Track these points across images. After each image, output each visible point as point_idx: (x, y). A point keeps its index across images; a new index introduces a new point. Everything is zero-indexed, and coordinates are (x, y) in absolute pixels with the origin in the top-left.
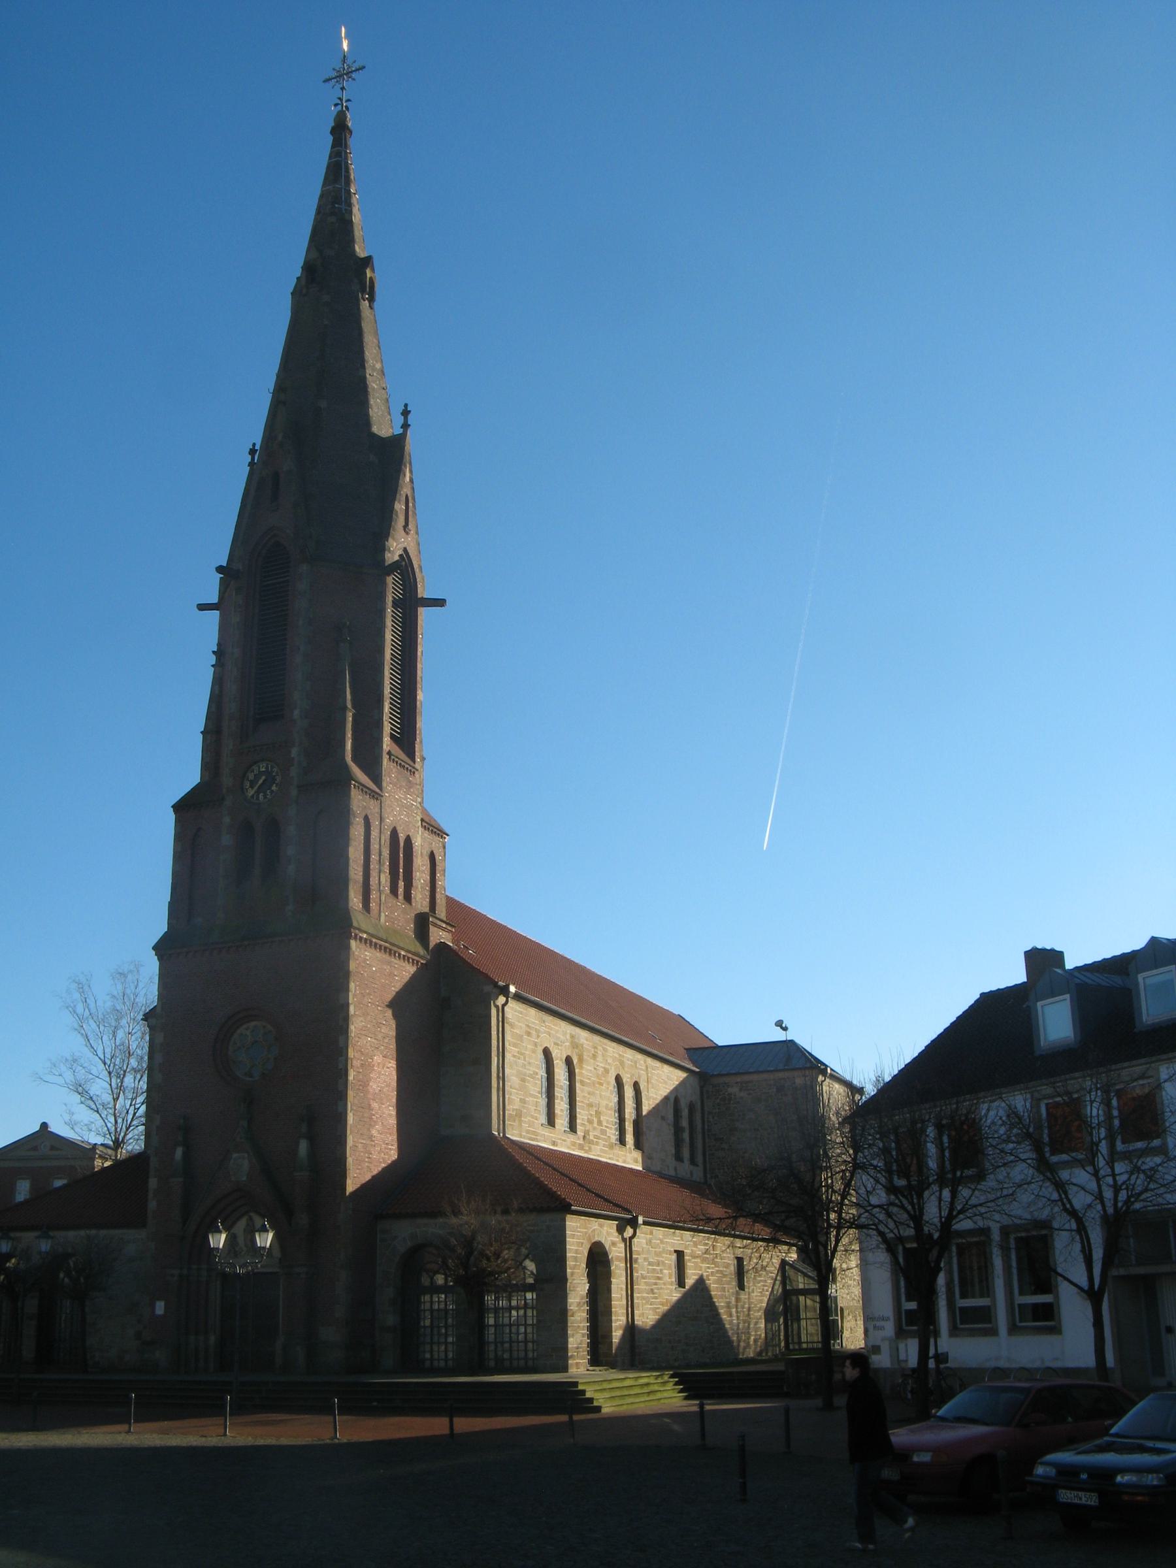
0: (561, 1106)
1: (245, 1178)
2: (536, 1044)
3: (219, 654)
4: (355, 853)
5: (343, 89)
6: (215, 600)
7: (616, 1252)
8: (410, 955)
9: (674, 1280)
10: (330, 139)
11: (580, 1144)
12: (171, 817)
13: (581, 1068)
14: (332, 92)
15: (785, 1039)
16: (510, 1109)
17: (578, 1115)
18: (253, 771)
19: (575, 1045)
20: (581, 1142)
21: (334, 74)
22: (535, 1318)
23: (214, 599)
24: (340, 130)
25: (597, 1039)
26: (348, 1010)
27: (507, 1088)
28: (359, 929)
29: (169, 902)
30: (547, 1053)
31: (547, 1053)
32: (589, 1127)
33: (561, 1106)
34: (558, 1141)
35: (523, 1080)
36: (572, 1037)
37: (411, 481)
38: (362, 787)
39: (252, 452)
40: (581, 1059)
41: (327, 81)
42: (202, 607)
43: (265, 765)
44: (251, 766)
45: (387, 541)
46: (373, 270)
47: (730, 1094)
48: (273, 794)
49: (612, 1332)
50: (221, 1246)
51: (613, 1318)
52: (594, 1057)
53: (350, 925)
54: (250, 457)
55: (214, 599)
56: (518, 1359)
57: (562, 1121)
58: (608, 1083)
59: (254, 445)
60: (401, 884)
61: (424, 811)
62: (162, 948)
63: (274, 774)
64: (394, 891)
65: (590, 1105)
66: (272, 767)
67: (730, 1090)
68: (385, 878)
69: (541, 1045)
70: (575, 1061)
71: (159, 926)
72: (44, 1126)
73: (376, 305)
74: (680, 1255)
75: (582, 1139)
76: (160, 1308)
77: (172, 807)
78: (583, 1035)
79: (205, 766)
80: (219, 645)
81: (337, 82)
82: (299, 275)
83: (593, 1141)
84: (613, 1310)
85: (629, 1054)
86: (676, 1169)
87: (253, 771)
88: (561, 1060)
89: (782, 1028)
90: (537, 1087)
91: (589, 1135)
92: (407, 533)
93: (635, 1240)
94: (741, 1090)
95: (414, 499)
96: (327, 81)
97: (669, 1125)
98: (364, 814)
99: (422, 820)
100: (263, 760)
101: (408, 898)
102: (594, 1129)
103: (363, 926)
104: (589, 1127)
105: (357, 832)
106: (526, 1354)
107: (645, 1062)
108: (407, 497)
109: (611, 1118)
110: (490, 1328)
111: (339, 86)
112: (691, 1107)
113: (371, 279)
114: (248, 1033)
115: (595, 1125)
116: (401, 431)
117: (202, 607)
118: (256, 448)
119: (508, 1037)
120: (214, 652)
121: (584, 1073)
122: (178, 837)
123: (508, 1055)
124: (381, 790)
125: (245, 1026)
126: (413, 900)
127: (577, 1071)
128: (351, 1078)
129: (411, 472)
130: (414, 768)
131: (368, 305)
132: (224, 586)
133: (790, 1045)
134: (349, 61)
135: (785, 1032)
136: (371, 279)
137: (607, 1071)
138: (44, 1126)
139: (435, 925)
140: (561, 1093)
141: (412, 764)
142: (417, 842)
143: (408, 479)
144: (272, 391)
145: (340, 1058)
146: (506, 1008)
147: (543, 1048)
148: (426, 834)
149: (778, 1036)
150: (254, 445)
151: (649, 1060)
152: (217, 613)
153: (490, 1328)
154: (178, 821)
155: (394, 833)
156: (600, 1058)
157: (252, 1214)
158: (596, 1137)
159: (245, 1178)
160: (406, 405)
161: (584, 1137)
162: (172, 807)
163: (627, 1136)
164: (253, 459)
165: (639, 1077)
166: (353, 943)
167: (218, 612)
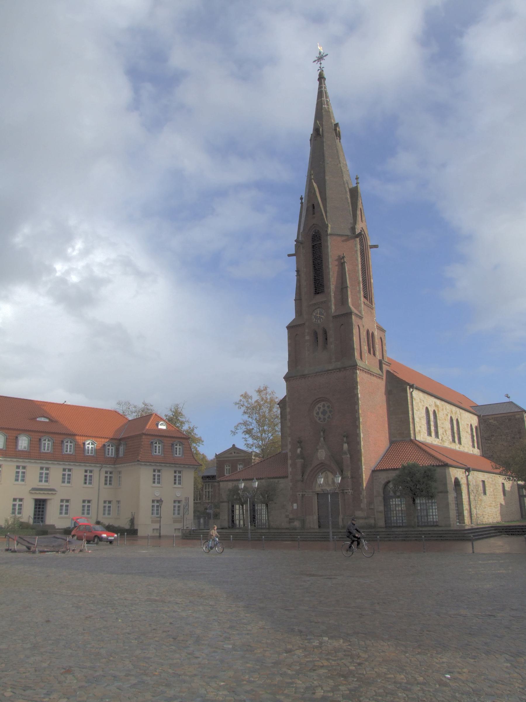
0: (433, 428)
1: (324, 459)
2: (423, 406)
3: (298, 271)
4: (356, 339)
5: (321, 64)
6: (294, 253)
7: (463, 482)
8: (377, 375)
9: (482, 491)
10: (318, 82)
11: (440, 442)
12: (286, 331)
13: (439, 414)
14: (317, 66)
15: (509, 401)
16: (417, 430)
17: (439, 432)
18: (315, 312)
19: (436, 406)
20: (441, 441)
21: (316, 59)
22: (266, 515)
23: (294, 252)
24: (321, 78)
25: (443, 403)
26: (358, 396)
27: (415, 422)
28: (360, 366)
29: (288, 361)
30: (427, 408)
31: (427, 408)
32: (443, 436)
33: (433, 428)
34: (432, 440)
35: (420, 419)
36: (435, 403)
37: (362, 203)
38: (356, 315)
39: (301, 199)
40: (438, 410)
41: (314, 61)
42: (289, 255)
43: (319, 310)
44: (314, 310)
45: (356, 225)
46: (339, 128)
47: (490, 423)
48: (323, 320)
49: (463, 511)
50: (339, 482)
51: (464, 506)
52: (443, 409)
53: (357, 365)
54: (301, 200)
55: (294, 252)
56: (394, 523)
57: (433, 434)
58: (448, 419)
59: (302, 196)
60: (372, 349)
61: (377, 323)
62: (287, 378)
63: (323, 313)
64: (369, 352)
65: (443, 428)
66: (322, 310)
67: (490, 421)
68: (365, 348)
69: (425, 406)
70: (437, 412)
71: (285, 370)
72: (234, 445)
73: (341, 140)
74: (483, 482)
75: (441, 440)
76: (295, 506)
77: (286, 327)
78: (438, 402)
79: (297, 312)
80: (297, 268)
81: (318, 61)
82: (312, 133)
83: (444, 441)
84: (463, 503)
85: (454, 409)
86: (473, 451)
87: (315, 312)
88: (432, 411)
89: (507, 397)
90: (424, 422)
91: (443, 439)
92: (362, 222)
93: (469, 477)
94: (494, 421)
95: (363, 210)
96: (314, 61)
97: (469, 434)
98: (357, 325)
99: (377, 326)
100: (319, 308)
101: (374, 354)
102: (445, 436)
103: (361, 366)
104: (443, 436)
105: (355, 331)
106: (397, 521)
107: (460, 412)
108: (361, 209)
109: (449, 432)
110: (430, 510)
111: (319, 63)
112: (476, 428)
113: (339, 131)
114: (321, 406)
115: (445, 435)
116: (356, 185)
117: (289, 255)
118: (302, 197)
119: (414, 403)
120: (296, 271)
121: (440, 415)
122: (290, 338)
123: (415, 410)
124: (362, 316)
125: (319, 404)
126: (376, 355)
127: (437, 415)
128: (361, 420)
129: (361, 199)
130: (372, 307)
131: (339, 141)
132: (297, 247)
133: (511, 403)
134: (322, 54)
135: (509, 399)
136: (339, 131)
137: (447, 415)
138: (234, 445)
139: (385, 364)
140: (432, 423)
141: (372, 306)
142: (376, 333)
143: (360, 202)
144: (307, 176)
145: (356, 414)
146: (413, 393)
147: (426, 407)
148: (378, 331)
149: (506, 400)
150: (302, 196)
151: (461, 411)
152: (295, 257)
153: (430, 510)
154: (289, 332)
155: (368, 331)
156: (444, 410)
157: (327, 472)
158: (445, 439)
159: (324, 459)
160: (357, 176)
161: (442, 440)
162: (286, 327)
163: (456, 439)
164: (302, 201)
165: (458, 417)
166: (358, 371)
167: (295, 257)
